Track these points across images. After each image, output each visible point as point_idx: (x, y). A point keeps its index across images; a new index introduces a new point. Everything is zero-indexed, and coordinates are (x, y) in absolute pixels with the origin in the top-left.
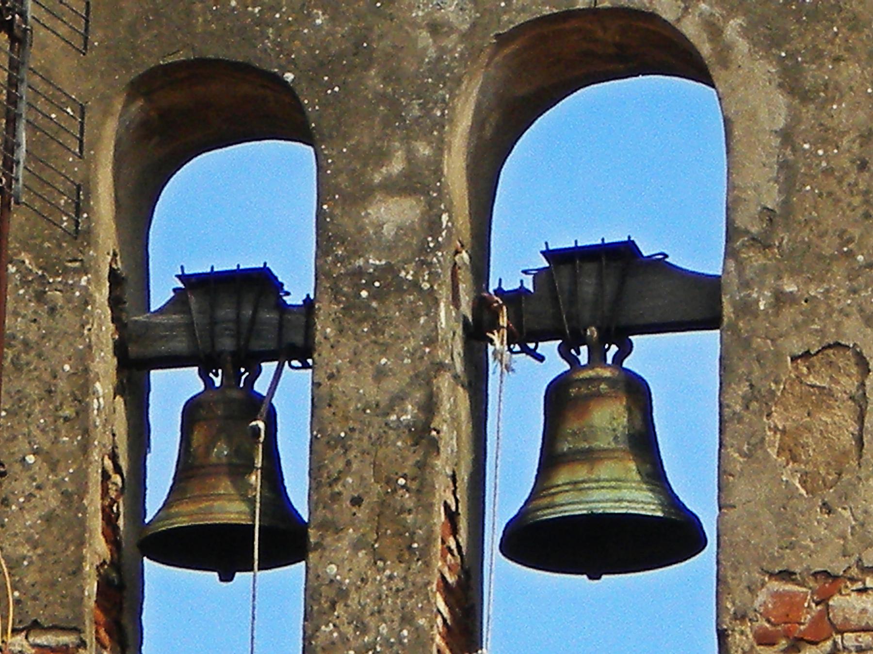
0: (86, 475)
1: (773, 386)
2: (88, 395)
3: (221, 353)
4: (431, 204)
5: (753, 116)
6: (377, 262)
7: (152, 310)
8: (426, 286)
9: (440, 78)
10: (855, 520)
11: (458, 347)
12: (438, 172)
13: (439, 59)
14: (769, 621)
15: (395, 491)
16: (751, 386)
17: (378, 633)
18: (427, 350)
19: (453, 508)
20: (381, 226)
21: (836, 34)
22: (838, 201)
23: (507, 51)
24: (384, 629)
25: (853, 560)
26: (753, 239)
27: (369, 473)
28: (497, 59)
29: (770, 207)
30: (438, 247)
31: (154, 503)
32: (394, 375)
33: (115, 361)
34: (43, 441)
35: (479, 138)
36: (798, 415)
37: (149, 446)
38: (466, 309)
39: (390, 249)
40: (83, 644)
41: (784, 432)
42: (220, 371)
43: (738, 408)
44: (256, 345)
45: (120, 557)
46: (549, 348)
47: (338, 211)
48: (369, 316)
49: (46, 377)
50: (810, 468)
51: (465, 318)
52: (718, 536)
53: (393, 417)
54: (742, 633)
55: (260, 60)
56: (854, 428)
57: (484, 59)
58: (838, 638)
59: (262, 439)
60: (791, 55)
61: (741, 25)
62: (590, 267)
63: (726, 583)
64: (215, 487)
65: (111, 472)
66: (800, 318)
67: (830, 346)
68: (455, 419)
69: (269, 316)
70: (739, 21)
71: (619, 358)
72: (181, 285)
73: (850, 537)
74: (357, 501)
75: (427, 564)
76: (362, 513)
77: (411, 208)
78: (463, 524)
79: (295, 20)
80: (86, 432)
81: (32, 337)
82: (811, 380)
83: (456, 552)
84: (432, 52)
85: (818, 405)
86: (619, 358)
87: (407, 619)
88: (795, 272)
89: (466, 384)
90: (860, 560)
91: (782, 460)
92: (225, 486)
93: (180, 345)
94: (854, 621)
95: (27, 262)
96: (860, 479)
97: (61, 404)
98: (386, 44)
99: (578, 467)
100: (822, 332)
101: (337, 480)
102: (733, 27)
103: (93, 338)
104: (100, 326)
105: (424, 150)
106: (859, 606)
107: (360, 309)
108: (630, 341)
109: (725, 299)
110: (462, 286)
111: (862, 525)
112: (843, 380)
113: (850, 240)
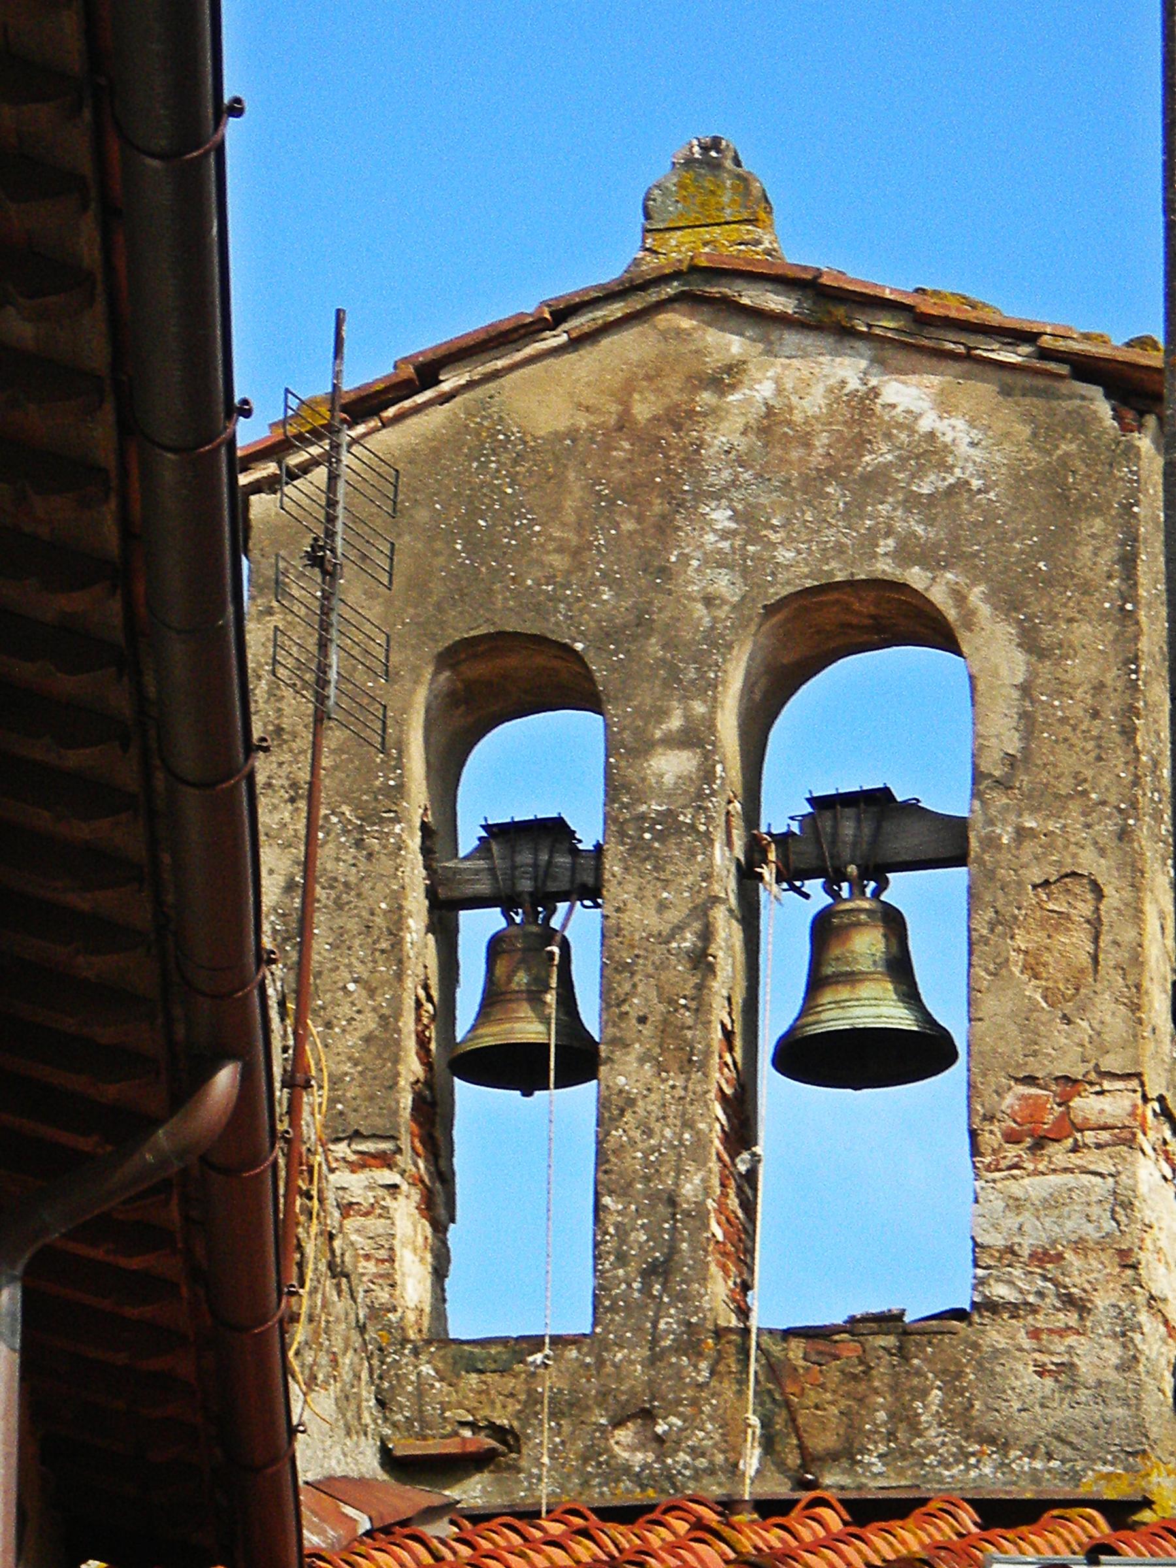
0: (401, 1002)
1: (1016, 912)
2: (401, 929)
3: (520, 894)
4: (706, 756)
5: (996, 674)
6: (659, 808)
7: (461, 854)
8: (702, 828)
9: (714, 644)
10: (1093, 1030)
11: (732, 884)
12: (712, 728)
13: (713, 628)
14: (1015, 1122)
15: (676, 1010)
16: (996, 912)
17: (663, 1136)
18: (704, 884)
19: (729, 1028)
20: (662, 776)
21: (1070, 598)
22: (1072, 746)
23: (774, 620)
24: (668, 1133)
25: (1091, 1065)
26: (997, 782)
27: (653, 996)
28: (763, 629)
29: (1011, 752)
30: (713, 793)
31: (460, 1033)
32: (675, 906)
33: (427, 903)
34: (361, 970)
35: (750, 700)
36: (1040, 937)
37: (457, 981)
38: (739, 853)
39: (669, 796)
40: (399, 1150)
41: (1026, 952)
42: (520, 911)
43: (985, 932)
44: (552, 887)
45: (433, 1077)
46: (814, 886)
47: (623, 763)
48: (651, 855)
49: (364, 914)
50: (1051, 984)
51: (738, 860)
52: (969, 1046)
53: (674, 945)
54: (991, 1132)
55: (553, 632)
56: (1090, 948)
57: (753, 628)
58: (1078, 1136)
59: (556, 962)
60: (1029, 618)
61: (983, 593)
62: (850, 812)
63: (975, 1087)
64: (514, 1011)
65: (424, 1001)
66: (1040, 850)
67: (1067, 876)
68: (730, 948)
69: (563, 860)
70: (982, 588)
71: (876, 893)
72: (484, 834)
73: (1088, 1046)
74: (642, 1020)
75: (706, 1075)
76: (647, 1030)
77: (689, 760)
78: (738, 1042)
79: (585, 596)
80: (400, 962)
81: (353, 880)
82: (1050, 906)
83: (732, 1067)
84: (707, 622)
85: (1056, 927)
86: (876, 893)
87: (688, 1124)
88: (1034, 810)
89: (739, 917)
90: (1097, 1065)
91: (1025, 977)
92: (525, 1010)
93: (483, 887)
94: (1093, 1122)
95: (347, 813)
96: (1095, 992)
97: (379, 938)
98: (665, 616)
99: (840, 988)
100: (1060, 863)
101: (624, 1001)
102: (976, 595)
103: (407, 880)
104: (413, 869)
105: (699, 708)
106: (1098, 1106)
107: (642, 849)
108: (887, 879)
109: (972, 836)
110: (735, 832)
111: (1099, 1034)
112: (1080, 905)
113: (1085, 780)
